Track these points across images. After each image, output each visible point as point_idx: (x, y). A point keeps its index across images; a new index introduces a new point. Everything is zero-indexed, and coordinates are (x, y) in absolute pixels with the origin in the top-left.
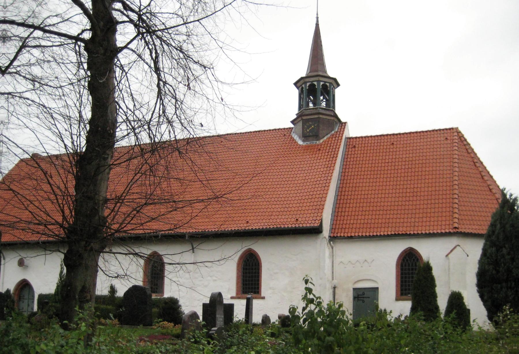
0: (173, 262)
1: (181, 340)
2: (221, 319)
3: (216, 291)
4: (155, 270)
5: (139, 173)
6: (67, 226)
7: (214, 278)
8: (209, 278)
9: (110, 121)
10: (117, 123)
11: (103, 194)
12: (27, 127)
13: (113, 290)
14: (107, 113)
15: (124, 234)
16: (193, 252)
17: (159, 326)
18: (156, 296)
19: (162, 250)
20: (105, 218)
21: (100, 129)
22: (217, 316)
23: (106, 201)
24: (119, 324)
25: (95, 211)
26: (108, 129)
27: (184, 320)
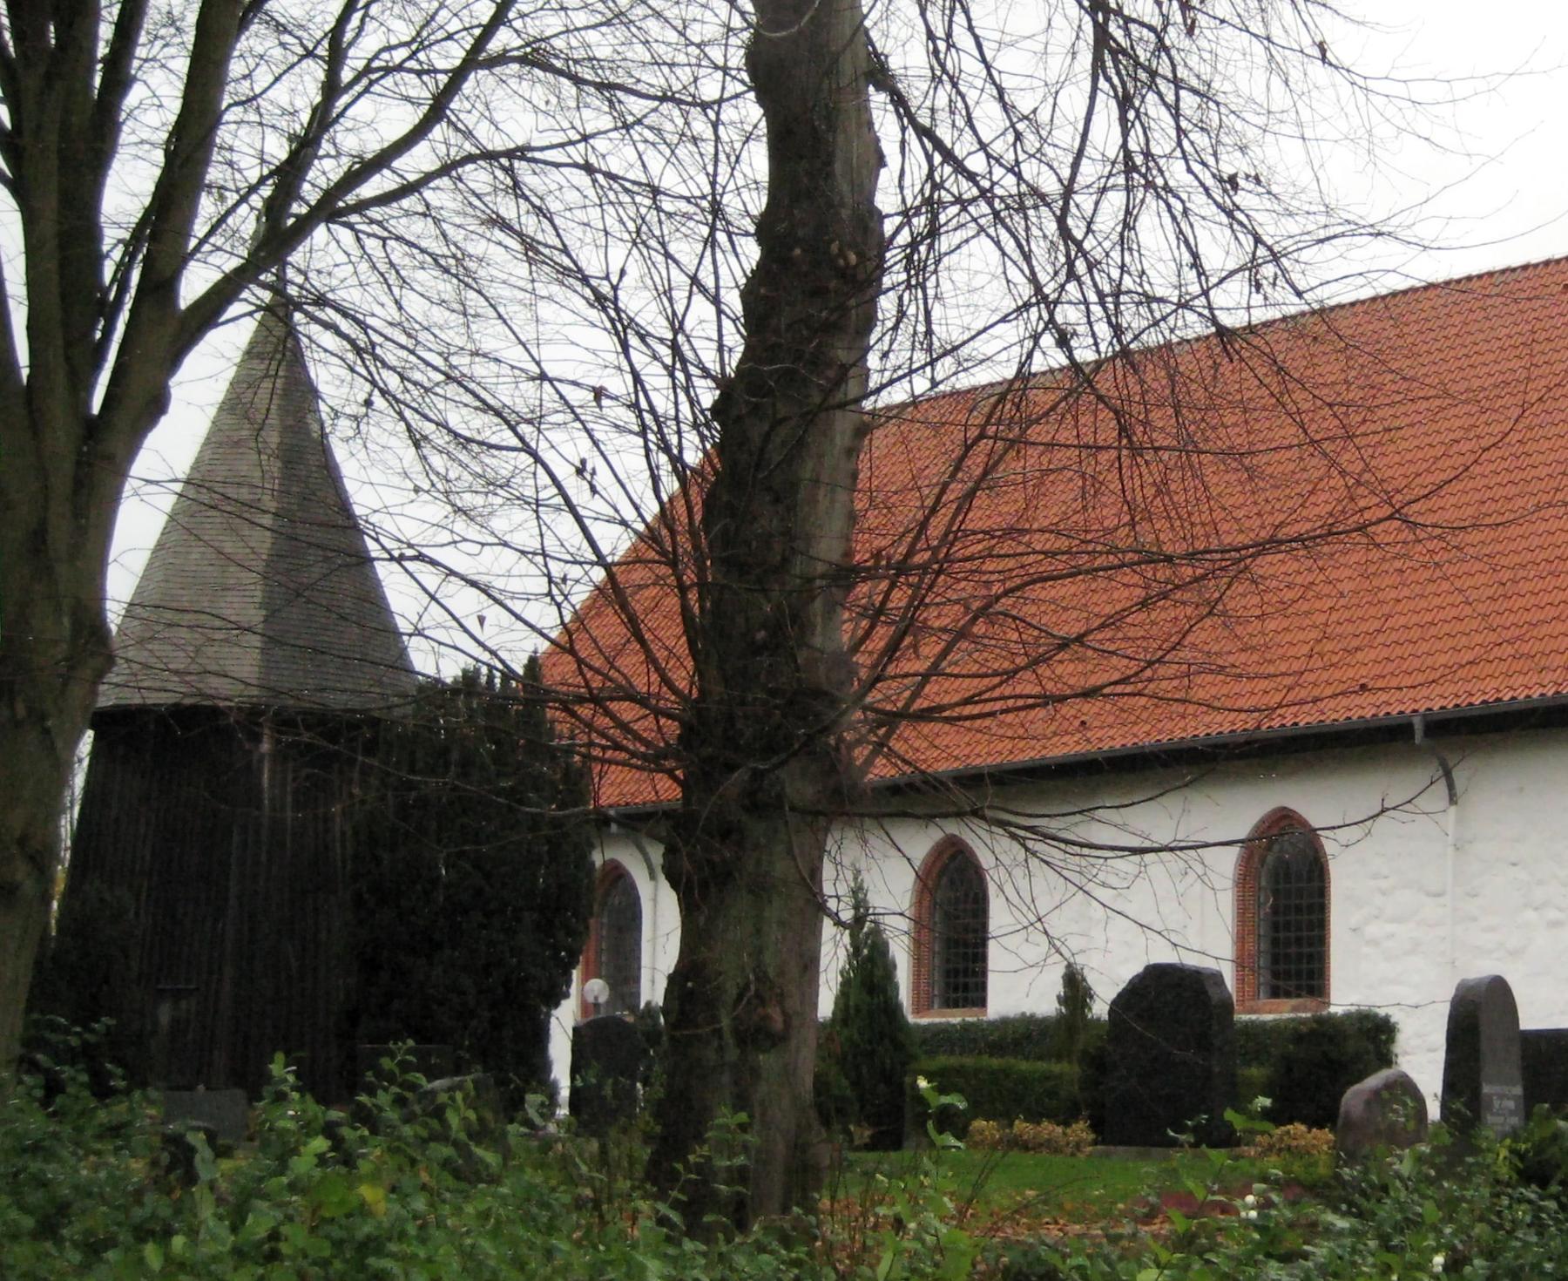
0: (1147, 844)
1: (703, 1142)
2: (1511, 1104)
3: (1480, 969)
4: (1289, 900)
5: (982, 436)
6: (669, 701)
7: (1553, 914)
8: (1530, 915)
9: (845, 213)
10: (882, 217)
11: (827, 549)
12: (1008, 281)
13: (1075, 989)
14: (829, 176)
15: (291, 702)
16: (1453, 799)
17: (1271, 1147)
18: (1295, 1009)
19: (1320, 802)
20: (842, 661)
21: (798, 251)
22: (1486, 1089)
23: (846, 575)
24: (1095, 1143)
25: (787, 631)
26: (834, 248)
27: (1347, 1113)
